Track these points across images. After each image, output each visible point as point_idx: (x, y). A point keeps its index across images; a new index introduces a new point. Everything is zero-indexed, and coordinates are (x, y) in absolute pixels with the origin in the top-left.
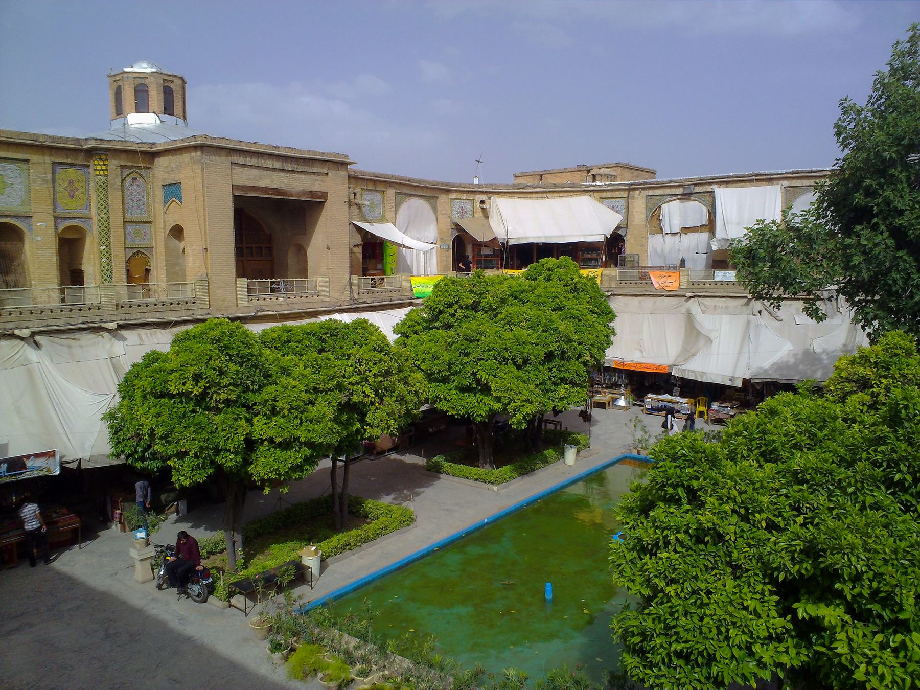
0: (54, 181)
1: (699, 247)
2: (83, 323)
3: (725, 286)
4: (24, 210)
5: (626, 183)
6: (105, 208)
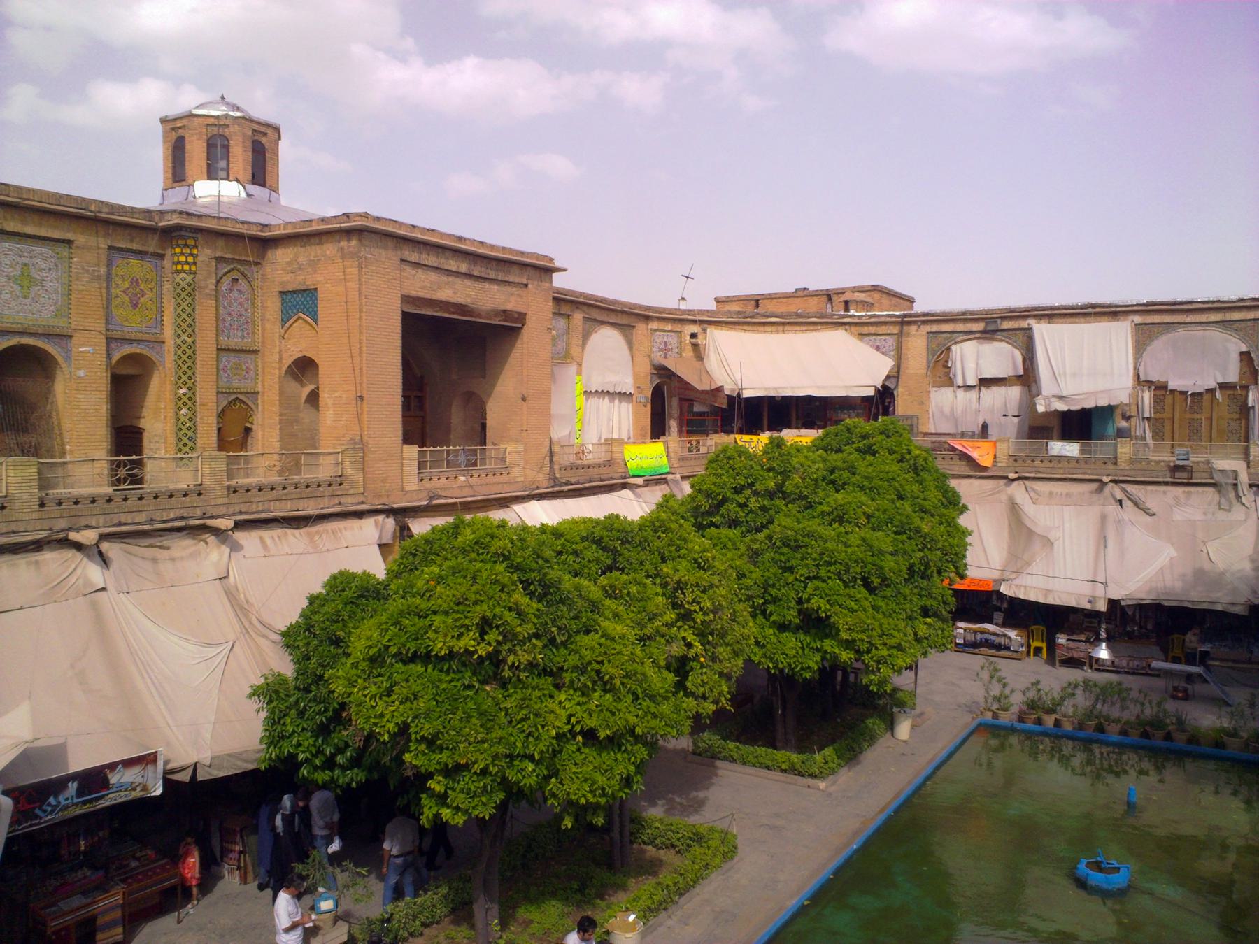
0: (109, 278)
1: (1008, 406)
2: (176, 519)
3: (1064, 464)
4: (60, 324)
5: (897, 313)
6: (189, 326)
